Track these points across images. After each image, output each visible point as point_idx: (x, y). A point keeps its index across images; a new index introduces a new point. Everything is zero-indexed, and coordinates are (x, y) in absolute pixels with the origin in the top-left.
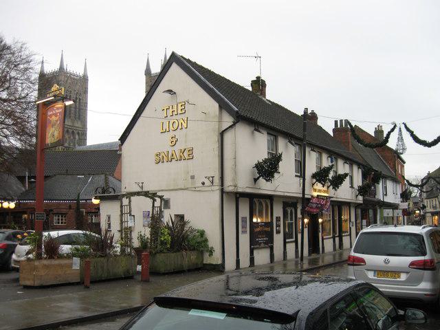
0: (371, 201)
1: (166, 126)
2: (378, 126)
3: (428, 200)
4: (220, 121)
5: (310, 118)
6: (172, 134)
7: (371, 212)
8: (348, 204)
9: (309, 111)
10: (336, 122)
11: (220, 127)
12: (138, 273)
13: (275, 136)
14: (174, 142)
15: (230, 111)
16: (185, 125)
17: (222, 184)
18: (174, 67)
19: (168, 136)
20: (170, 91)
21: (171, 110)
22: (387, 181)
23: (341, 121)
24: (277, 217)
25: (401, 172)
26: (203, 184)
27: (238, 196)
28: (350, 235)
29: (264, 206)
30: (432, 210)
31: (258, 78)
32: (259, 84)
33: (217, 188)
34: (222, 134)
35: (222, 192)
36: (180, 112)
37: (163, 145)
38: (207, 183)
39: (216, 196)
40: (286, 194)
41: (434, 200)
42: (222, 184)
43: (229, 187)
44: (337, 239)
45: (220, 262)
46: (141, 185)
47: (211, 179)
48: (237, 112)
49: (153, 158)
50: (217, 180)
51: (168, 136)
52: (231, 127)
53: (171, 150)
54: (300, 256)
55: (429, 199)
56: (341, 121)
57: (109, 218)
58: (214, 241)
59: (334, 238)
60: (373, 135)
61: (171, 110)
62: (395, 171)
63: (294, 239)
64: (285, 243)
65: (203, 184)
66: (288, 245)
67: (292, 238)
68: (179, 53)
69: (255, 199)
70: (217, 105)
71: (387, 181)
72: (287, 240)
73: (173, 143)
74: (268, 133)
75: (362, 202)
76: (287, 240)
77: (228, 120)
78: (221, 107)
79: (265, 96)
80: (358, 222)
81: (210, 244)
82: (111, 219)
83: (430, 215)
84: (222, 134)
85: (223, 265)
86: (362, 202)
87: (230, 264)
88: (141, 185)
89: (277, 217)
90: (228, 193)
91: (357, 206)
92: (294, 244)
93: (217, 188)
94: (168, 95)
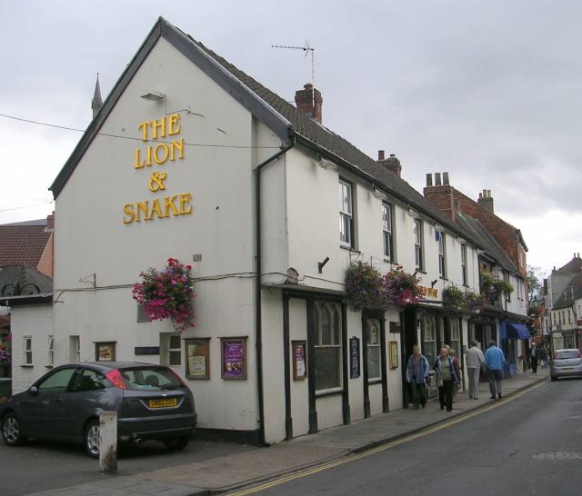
1: (146, 156)
3: (557, 312)
4: (255, 147)
7: (489, 329)
9: (387, 156)
10: (429, 177)
11: (255, 156)
12: (477, 315)
13: (351, 184)
14: (158, 187)
15: (275, 126)
18: (163, 43)
19: (147, 175)
22: (511, 277)
23: (438, 175)
31: (308, 86)
32: (309, 99)
34: (258, 172)
35: (259, 287)
37: (139, 191)
41: (566, 310)
43: (274, 278)
48: (289, 129)
51: (147, 175)
52: (277, 156)
53: (151, 198)
54: (467, 387)
55: (558, 309)
56: (438, 175)
57: (29, 342)
60: (476, 201)
62: (518, 264)
63: (380, 379)
64: (313, 398)
67: (338, 385)
68: (174, 21)
69: (316, 303)
70: (246, 117)
72: (317, 392)
74: (341, 178)
77: (271, 144)
78: (255, 119)
79: (321, 123)
82: (33, 344)
85: (261, 431)
87: (274, 430)
89: (245, 378)
90: (271, 288)
92: (380, 386)
94: (151, 103)
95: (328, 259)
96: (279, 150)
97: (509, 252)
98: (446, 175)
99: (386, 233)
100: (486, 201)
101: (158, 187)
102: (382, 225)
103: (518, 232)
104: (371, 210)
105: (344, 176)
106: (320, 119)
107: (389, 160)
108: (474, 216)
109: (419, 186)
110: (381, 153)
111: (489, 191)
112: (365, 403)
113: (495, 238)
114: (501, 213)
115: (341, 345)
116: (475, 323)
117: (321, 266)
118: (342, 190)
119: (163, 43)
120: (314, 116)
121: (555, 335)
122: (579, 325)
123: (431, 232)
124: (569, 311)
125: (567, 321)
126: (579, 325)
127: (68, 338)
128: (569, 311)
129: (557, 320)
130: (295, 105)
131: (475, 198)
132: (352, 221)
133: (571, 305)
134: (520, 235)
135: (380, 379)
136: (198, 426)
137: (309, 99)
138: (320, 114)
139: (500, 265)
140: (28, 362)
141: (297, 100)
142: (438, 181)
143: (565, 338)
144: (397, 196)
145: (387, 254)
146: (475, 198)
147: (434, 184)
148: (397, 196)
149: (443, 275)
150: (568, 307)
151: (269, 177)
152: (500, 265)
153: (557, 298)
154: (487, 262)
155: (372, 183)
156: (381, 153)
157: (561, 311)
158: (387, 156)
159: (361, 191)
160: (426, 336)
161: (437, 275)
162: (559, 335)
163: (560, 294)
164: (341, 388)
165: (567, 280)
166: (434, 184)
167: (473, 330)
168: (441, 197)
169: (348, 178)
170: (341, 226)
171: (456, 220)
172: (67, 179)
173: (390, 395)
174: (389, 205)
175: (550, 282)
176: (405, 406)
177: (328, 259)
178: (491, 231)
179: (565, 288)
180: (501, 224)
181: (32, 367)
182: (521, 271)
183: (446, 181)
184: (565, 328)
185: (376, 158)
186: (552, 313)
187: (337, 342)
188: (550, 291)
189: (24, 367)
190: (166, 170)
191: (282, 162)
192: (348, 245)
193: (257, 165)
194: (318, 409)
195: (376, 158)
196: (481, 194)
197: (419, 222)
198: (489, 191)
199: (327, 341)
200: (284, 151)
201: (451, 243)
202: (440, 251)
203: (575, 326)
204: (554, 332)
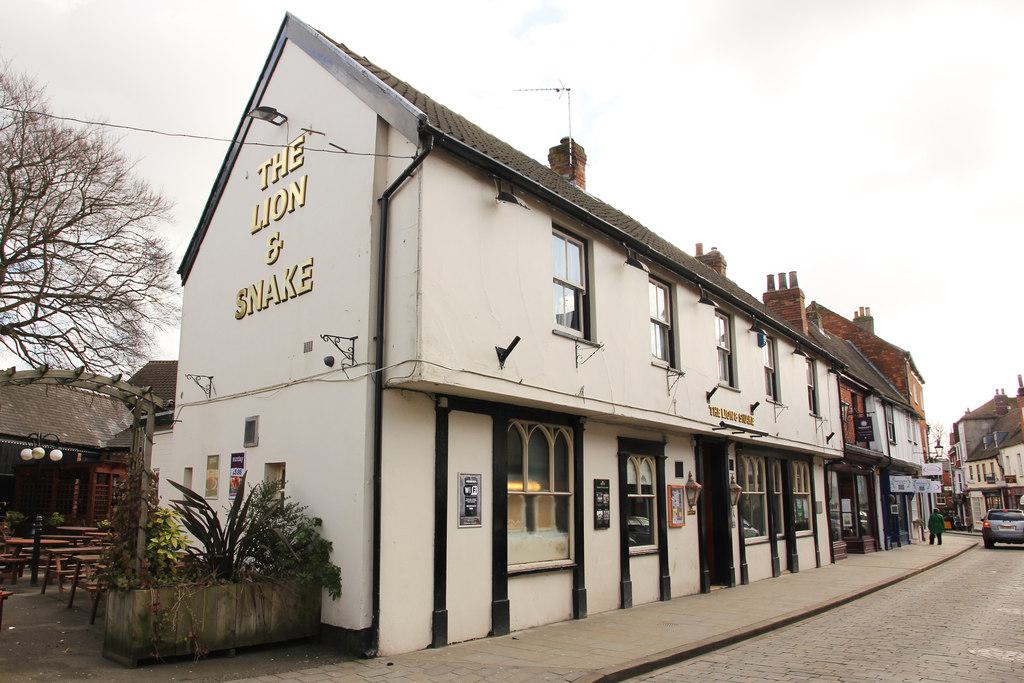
0: (861, 455)
3: (974, 465)
8: (808, 458)
10: (770, 279)
16: (299, 200)
21: (276, 165)
22: (895, 413)
23: (782, 276)
24: (597, 482)
25: (919, 400)
26: (330, 362)
27: (444, 403)
28: (815, 534)
29: (552, 443)
30: (985, 485)
31: (565, 141)
32: (568, 155)
33: (364, 370)
34: (385, 202)
35: (380, 385)
36: (292, 165)
39: (360, 393)
40: (619, 411)
41: (987, 463)
44: (781, 545)
45: (361, 622)
46: (205, 382)
49: (233, 307)
50: (364, 350)
53: (267, 274)
56: (782, 276)
58: (349, 554)
59: (773, 542)
62: (908, 396)
63: (654, 547)
65: (330, 362)
67: (651, 542)
68: (312, 17)
73: (274, 255)
74: (555, 226)
75: (841, 454)
76: (632, 549)
80: (832, 502)
81: (336, 559)
83: (979, 494)
84: (385, 202)
86: (841, 454)
88: (205, 382)
89: (597, 482)
91: (831, 463)
92: (812, 538)
93: (363, 373)
95: (517, 339)
97: (895, 381)
98: (793, 275)
99: (767, 369)
100: (864, 321)
102: (805, 384)
103: (907, 355)
104: (701, 325)
105: (658, 274)
106: (582, 183)
108: (846, 337)
109: (757, 290)
110: (699, 248)
114: (883, 331)
115: (655, 495)
116: (837, 472)
117: (503, 355)
118: (718, 326)
120: (573, 177)
124: (992, 464)
125: (975, 476)
127: (264, 466)
128: (992, 464)
131: (851, 318)
132: (730, 357)
133: (995, 456)
134: (910, 361)
135: (569, 562)
136: (322, 621)
137: (568, 155)
138: (583, 176)
139: (877, 394)
141: (550, 159)
142: (783, 284)
144: (729, 302)
145: (665, 359)
146: (851, 318)
147: (777, 288)
148: (729, 302)
149: (815, 412)
150: (990, 458)
151: (400, 205)
152: (877, 394)
153: (973, 446)
154: (856, 392)
155: (621, 240)
156: (699, 248)
157: (980, 463)
158: (706, 251)
159: (683, 296)
161: (714, 372)
166: (777, 288)
167: (834, 482)
168: (787, 303)
169: (665, 278)
170: (655, 340)
171: (809, 333)
172: (194, 239)
174: (811, 362)
177: (517, 339)
178: (868, 355)
180: (882, 346)
182: (913, 405)
183: (794, 282)
186: (967, 465)
191: (415, 181)
192: (579, 334)
196: (856, 313)
200: (418, 162)
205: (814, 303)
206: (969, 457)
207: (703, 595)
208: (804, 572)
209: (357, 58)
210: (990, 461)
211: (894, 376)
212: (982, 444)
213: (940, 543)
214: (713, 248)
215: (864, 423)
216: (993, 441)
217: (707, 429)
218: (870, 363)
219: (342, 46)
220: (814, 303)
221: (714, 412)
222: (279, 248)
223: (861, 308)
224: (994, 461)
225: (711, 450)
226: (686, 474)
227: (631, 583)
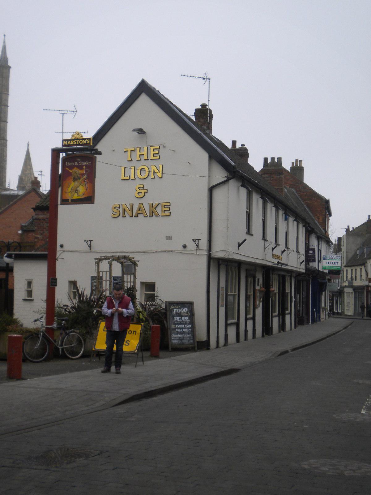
2: (297, 160)
3: (349, 269)
5: (243, 153)
6: (139, 183)
9: (238, 146)
14: (143, 193)
17: (210, 249)
18: (144, 99)
20: (141, 131)
21: (138, 153)
22: (322, 243)
31: (204, 106)
34: (211, 190)
35: (210, 258)
38: (191, 246)
41: (358, 269)
42: (210, 249)
43: (219, 251)
45: (205, 339)
47: (197, 242)
52: (223, 183)
60: (288, 169)
61: (138, 153)
66: (229, 328)
67: (233, 318)
68: (152, 83)
70: (205, 156)
71: (322, 243)
73: (141, 195)
75: (304, 271)
78: (210, 157)
79: (211, 133)
96: (225, 179)
97: (319, 219)
99: (263, 219)
101: (143, 193)
107: (240, 149)
110: (234, 143)
111: (301, 161)
112: (225, 335)
113: (308, 206)
114: (310, 179)
117: (239, 245)
119: (144, 99)
121: (347, 290)
122: (370, 282)
123: (283, 217)
124: (361, 269)
126: (370, 282)
128: (361, 269)
129: (349, 277)
130: (193, 118)
133: (364, 264)
140: (28, 297)
141: (196, 115)
143: (355, 293)
150: (361, 265)
153: (350, 256)
156: (234, 143)
157: (354, 269)
158: (238, 146)
160: (249, 291)
162: (350, 290)
163: (353, 253)
164: (235, 321)
165: (359, 241)
173: (220, 334)
175: (344, 242)
176: (263, 336)
179: (358, 247)
181: (32, 300)
184: (358, 283)
185: (230, 146)
187: (235, 292)
188: (344, 249)
189: (25, 300)
190: (148, 184)
193: (211, 186)
194: (228, 332)
195: (230, 146)
196: (293, 163)
197: (265, 203)
198: (301, 161)
199: (231, 291)
201: (302, 228)
202: (247, 209)
203: (366, 283)
204: (346, 286)
205: (353, 228)
206: (347, 264)
207: (217, 349)
208: (258, 338)
209: (165, 98)
210: (360, 267)
211: (318, 215)
212: (356, 254)
213: (118, 372)
214: (242, 145)
215: (311, 252)
216: (363, 253)
217: (271, 264)
218: (305, 206)
219: (215, 137)
220: (353, 228)
221: (274, 256)
222: (145, 192)
223: (297, 160)
224: (363, 267)
225: (267, 271)
226: (260, 284)
227: (228, 334)
